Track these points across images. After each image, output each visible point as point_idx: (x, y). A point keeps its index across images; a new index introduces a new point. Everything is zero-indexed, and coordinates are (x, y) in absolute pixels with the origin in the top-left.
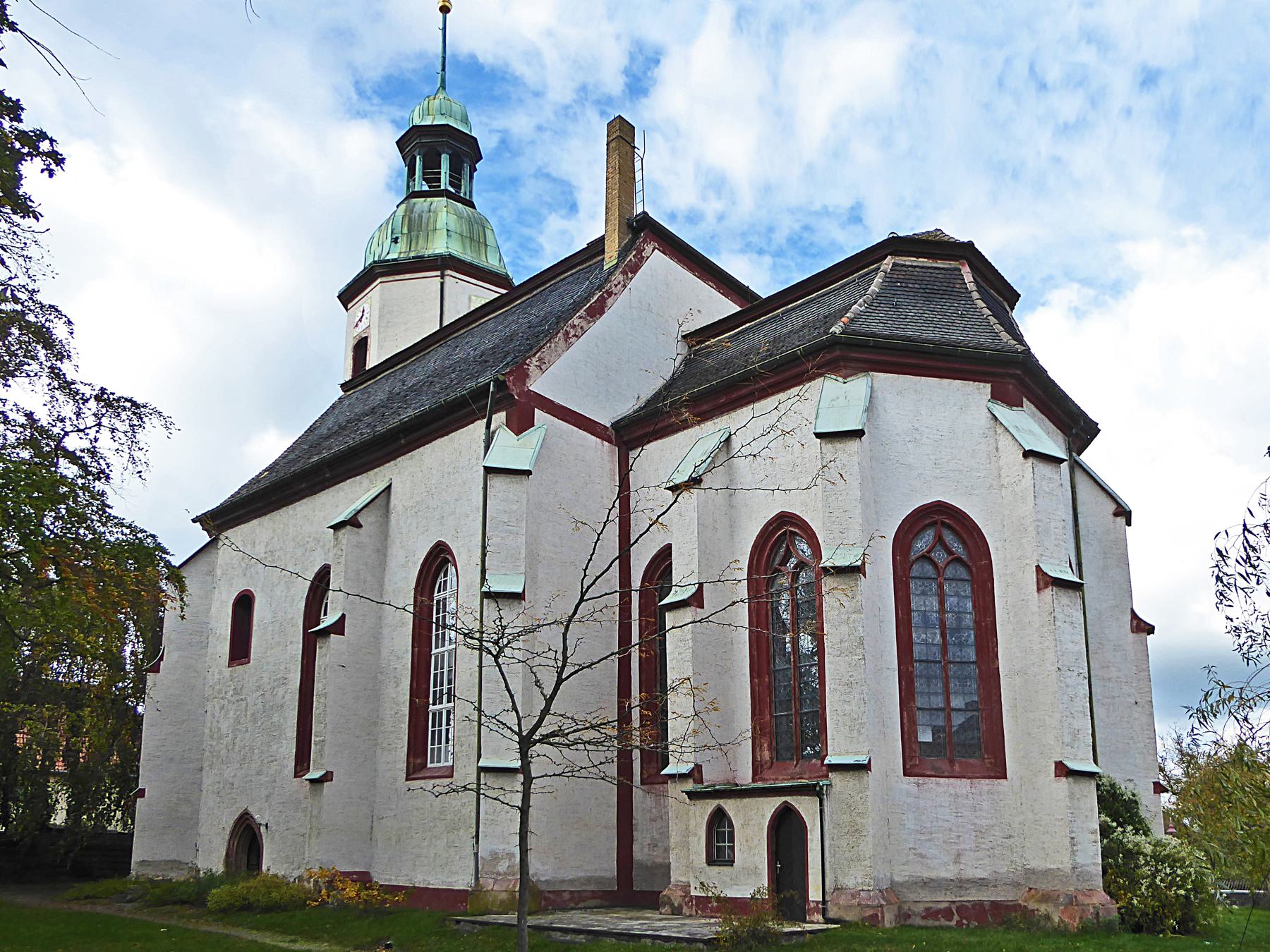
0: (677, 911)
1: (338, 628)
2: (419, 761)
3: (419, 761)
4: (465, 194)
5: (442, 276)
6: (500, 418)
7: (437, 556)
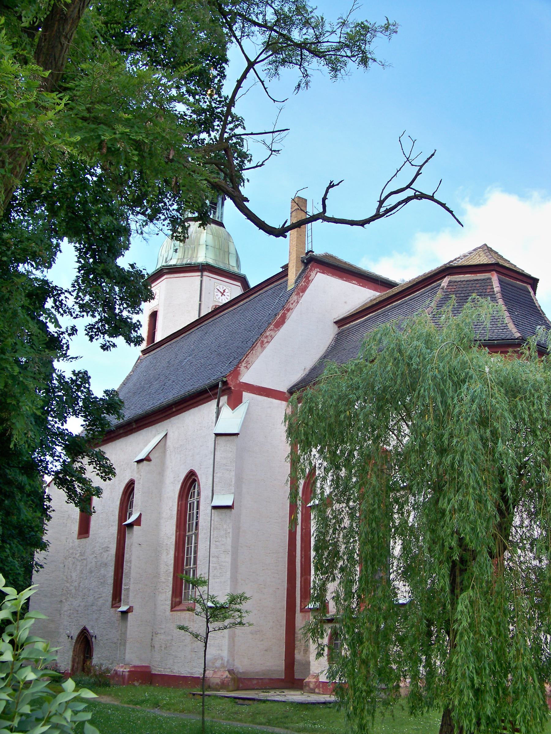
0: (312, 691)
1: (138, 522)
2: (178, 600)
3: (178, 600)
4: (218, 218)
5: (202, 276)
6: (224, 399)
7: (190, 478)
